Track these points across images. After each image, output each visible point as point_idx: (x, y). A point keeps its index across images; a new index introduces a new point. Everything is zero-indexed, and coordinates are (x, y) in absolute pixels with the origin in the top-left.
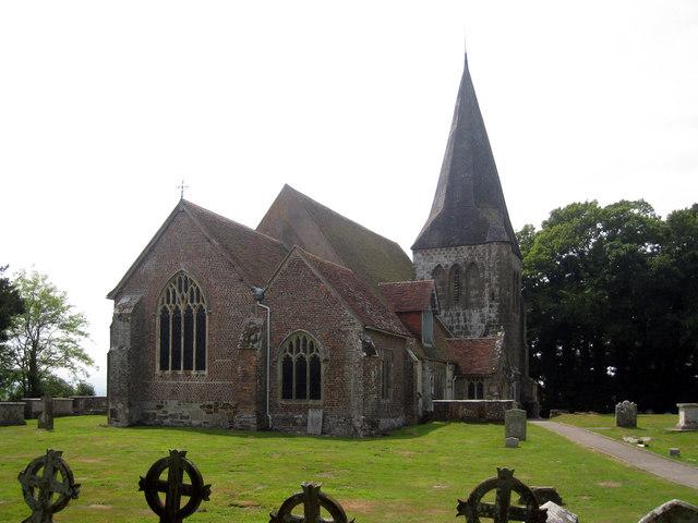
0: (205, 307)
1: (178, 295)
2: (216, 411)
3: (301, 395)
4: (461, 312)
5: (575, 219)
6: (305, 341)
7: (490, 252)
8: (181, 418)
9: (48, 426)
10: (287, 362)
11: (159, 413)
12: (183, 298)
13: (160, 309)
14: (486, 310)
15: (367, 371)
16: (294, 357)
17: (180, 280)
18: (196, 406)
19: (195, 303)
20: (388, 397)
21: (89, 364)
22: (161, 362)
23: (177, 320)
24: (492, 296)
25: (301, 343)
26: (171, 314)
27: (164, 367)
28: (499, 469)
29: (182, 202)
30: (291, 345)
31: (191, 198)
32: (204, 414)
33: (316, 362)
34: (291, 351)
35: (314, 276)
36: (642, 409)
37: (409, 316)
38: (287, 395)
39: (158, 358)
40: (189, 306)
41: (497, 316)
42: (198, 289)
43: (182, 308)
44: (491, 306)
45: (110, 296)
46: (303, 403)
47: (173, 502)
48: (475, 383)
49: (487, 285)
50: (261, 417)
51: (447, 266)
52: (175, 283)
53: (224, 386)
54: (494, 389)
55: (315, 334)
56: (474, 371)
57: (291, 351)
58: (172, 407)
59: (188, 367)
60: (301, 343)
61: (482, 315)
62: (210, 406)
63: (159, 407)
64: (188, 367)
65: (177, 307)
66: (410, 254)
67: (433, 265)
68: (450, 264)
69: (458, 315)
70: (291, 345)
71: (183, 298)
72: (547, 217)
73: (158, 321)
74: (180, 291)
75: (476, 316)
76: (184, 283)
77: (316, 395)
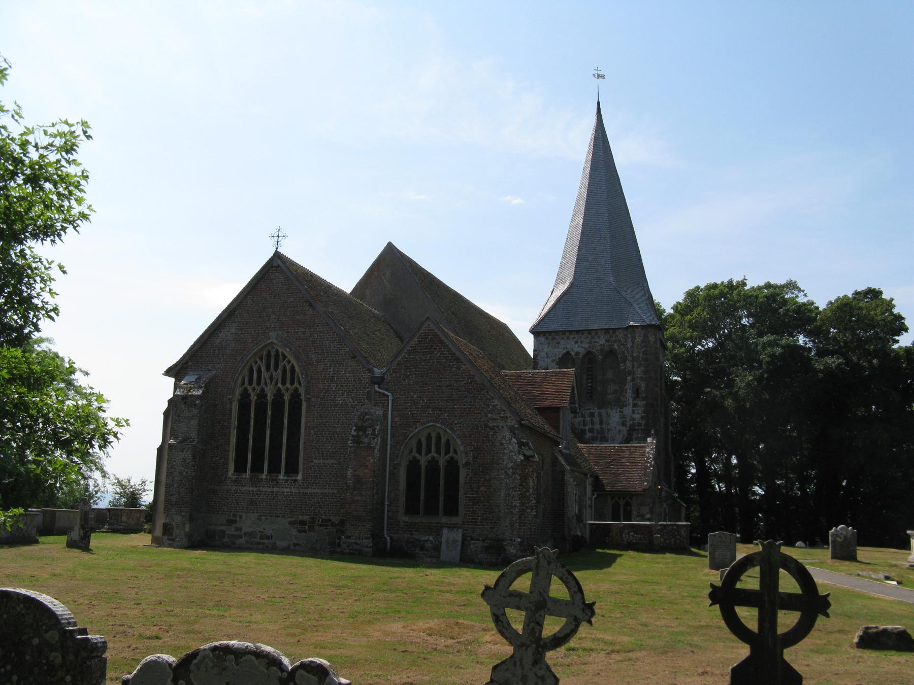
0: (302, 390)
2: (311, 528)
3: (431, 509)
4: (597, 411)
5: (716, 303)
6: (439, 438)
7: (634, 338)
8: (262, 537)
9: (82, 544)
10: (413, 466)
11: (231, 530)
12: (271, 378)
13: (238, 391)
14: (628, 410)
15: (524, 478)
16: (423, 460)
17: (269, 355)
19: (288, 385)
21: (130, 461)
22: (237, 461)
24: (637, 392)
25: (434, 440)
26: (253, 398)
27: (240, 467)
28: (711, 605)
29: (277, 256)
30: (419, 443)
31: (291, 252)
33: (453, 466)
34: (419, 451)
35: (453, 354)
37: (551, 413)
38: (412, 509)
39: (232, 455)
40: (279, 390)
42: (293, 369)
44: (635, 405)
45: (168, 373)
47: (570, 580)
48: (622, 502)
49: (629, 378)
50: (376, 536)
51: (577, 353)
52: (261, 358)
54: (645, 510)
55: (452, 429)
56: (619, 487)
57: (419, 451)
58: (248, 523)
59: (274, 469)
60: (434, 440)
62: (303, 523)
63: (231, 522)
64: (274, 469)
65: (263, 390)
66: (528, 343)
68: (582, 351)
69: (592, 415)
70: (419, 443)
71: (271, 378)
72: (680, 298)
73: (235, 407)
74: (268, 368)
75: (615, 417)
76: (272, 359)
77: (452, 509)
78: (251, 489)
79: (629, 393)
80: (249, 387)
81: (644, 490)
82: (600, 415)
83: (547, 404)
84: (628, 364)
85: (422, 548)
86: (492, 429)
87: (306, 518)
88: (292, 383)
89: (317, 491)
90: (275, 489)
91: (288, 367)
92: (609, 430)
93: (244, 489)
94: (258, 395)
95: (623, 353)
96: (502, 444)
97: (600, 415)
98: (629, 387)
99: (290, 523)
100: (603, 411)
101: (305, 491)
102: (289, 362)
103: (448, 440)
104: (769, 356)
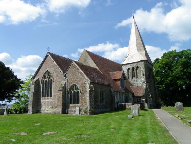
0: (52, 79)
1: (47, 77)
14: (142, 78)
18: (49, 107)
20: (103, 103)
22: (47, 95)
23: (46, 83)
24: (143, 74)
26: (45, 81)
32: (51, 109)
36: (185, 105)
43: (47, 80)
46: (75, 105)
49: (141, 72)
51: (131, 68)
53: (56, 101)
61: (141, 80)
62: (52, 107)
65: (46, 80)
67: (127, 68)
68: (132, 67)
69: (135, 80)
72: (162, 55)
74: (47, 76)
77: (78, 103)
79: (142, 75)
82: (136, 80)
84: (141, 69)
85: (73, 112)
86: (85, 84)
87: (53, 106)
94: (45, 81)
98: (142, 73)
99: (51, 107)
100: (137, 79)
104: (181, 65)
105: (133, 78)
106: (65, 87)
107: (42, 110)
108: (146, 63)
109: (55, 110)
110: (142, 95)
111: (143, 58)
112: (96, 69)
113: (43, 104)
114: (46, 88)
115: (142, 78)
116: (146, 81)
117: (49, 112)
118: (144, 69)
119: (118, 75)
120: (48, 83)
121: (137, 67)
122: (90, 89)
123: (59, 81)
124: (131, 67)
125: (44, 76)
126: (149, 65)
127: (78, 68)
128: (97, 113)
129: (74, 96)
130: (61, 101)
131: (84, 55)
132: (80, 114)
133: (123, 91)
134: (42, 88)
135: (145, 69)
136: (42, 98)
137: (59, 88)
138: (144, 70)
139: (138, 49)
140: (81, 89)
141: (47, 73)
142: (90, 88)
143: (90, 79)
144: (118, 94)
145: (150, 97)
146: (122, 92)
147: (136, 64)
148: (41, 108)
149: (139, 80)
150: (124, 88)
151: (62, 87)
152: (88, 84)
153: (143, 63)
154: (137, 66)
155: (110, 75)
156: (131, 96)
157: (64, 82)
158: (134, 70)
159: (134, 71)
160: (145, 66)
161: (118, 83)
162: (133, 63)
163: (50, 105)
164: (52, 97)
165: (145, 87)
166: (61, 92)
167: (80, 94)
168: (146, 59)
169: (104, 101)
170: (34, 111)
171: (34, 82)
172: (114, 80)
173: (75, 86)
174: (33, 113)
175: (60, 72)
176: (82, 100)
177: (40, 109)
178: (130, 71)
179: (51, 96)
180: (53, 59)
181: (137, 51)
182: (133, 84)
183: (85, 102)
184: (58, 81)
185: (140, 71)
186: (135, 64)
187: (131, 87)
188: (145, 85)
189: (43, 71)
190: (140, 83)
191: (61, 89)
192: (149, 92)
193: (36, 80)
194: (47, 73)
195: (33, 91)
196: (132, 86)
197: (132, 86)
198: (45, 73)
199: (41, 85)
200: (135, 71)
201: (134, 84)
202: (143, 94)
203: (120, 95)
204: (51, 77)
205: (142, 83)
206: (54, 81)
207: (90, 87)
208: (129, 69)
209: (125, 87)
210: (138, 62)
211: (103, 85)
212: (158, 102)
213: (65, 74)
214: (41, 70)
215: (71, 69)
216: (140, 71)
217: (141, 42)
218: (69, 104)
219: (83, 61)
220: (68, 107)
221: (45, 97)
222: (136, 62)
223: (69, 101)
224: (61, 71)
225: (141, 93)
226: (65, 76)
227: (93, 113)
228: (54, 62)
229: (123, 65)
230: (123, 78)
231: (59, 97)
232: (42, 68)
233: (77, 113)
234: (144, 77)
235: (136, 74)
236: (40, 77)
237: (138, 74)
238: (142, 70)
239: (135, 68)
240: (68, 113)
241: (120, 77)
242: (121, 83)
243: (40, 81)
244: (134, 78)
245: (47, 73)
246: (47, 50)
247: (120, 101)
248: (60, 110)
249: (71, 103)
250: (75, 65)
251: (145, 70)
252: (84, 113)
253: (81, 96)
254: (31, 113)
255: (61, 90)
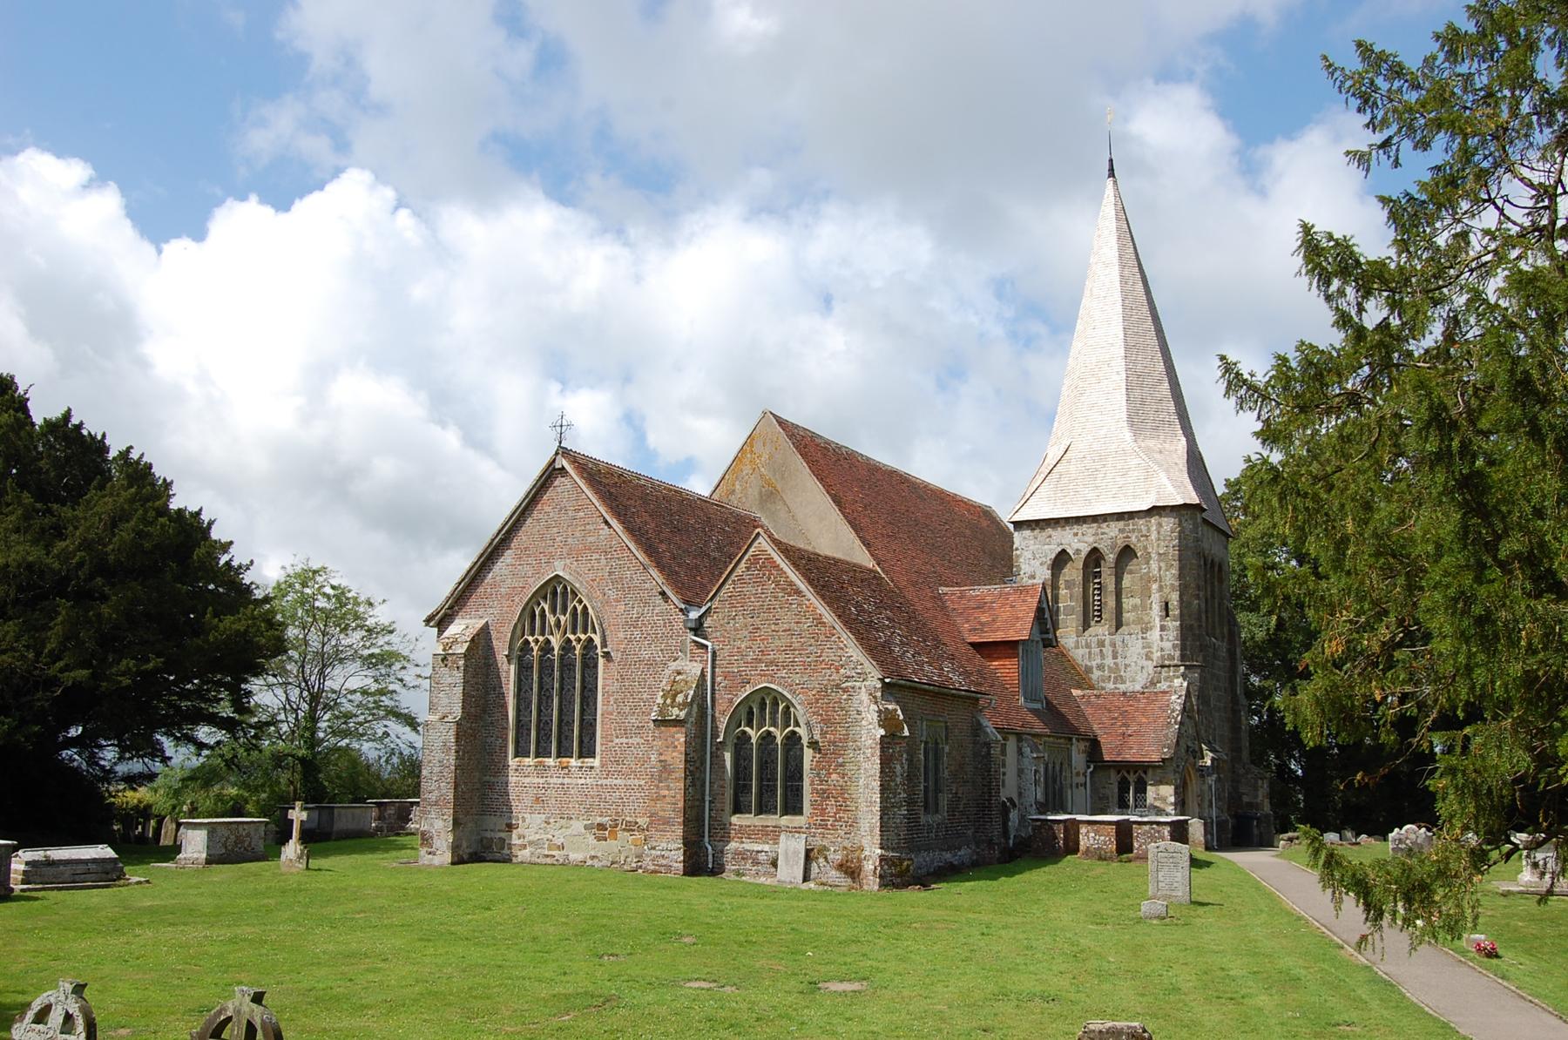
0: (597, 640)
1: (551, 619)
14: (1155, 634)
18: (578, 826)
22: (517, 743)
23: (545, 666)
32: (591, 839)
40: (569, 640)
41: (1174, 646)
43: (556, 642)
44: (1163, 628)
48: (1132, 778)
49: (1155, 586)
51: (1078, 551)
61: (1147, 646)
62: (601, 827)
67: (1052, 551)
68: (1085, 549)
69: (1101, 644)
74: (554, 611)
78: (536, 780)
80: (531, 639)
81: (1164, 760)
82: (1113, 645)
83: (998, 636)
84: (1154, 565)
85: (756, 863)
86: (845, 690)
87: (604, 820)
88: (585, 632)
89: (618, 782)
90: (566, 781)
91: (580, 608)
92: (1126, 666)
93: (527, 780)
94: (541, 649)
95: (1145, 548)
96: (859, 713)
97: (1113, 645)
99: (586, 827)
100: (1117, 638)
101: (604, 782)
102: (580, 601)
103: (787, 708)
105: (1086, 626)
106: (701, 706)
107: (515, 841)
108: (1189, 526)
109: (621, 846)
110: (1155, 757)
111: (1170, 488)
112: (877, 577)
113: (528, 801)
114: (550, 697)
115: (1155, 634)
116: (1183, 658)
117: (576, 856)
118: (1175, 571)
119: (1005, 614)
120: (567, 666)
121: (1127, 553)
122: (882, 732)
123: (648, 655)
124: (1076, 546)
125: (529, 615)
126: (1211, 544)
127: (791, 584)
128: (924, 879)
129: (766, 764)
130: (675, 790)
131: (758, 447)
132: (806, 878)
133: (1039, 727)
134: (531, 694)
135: (1181, 569)
136: (513, 762)
137: (663, 709)
138: (1171, 576)
139: (1137, 420)
140: (814, 720)
141: (555, 593)
142: (886, 719)
143: (882, 664)
144: (1012, 744)
145: (1203, 772)
146: (1034, 735)
147: (1121, 524)
148: (510, 827)
149: (1135, 648)
150: (1038, 706)
151: (680, 699)
152: (864, 697)
153: (1169, 524)
154: (1120, 544)
155: (944, 608)
156: (1078, 757)
157: (695, 669)
158: (1101, 569)
159: (1098, 575)
160: (1182, 548)
161: (1006, 669)
162: (1095, 519)
163: (582, 813)
164: (596, 762)
165: (1176, 701)
166: (681, 738)
167: (808, 754)
168: (1194, 498)
169: (944, 800)
170: (465, 845)
171: (461, 649)
172: (978, 647)
173: (775, 704)
174: (461, 858)
175: (659, 600)
176: (824, 795)
177: (503, 835)
178: (1073, 572)
179: (587, 751)
180: (597, 492)
181: (1128, 435)
182: (1089, 670)
183: (840, 808)
184: (645, 654)
185: (1148, 580)
186: (1112, 530)
187: (1075, 692)
188: (1180, 684)
189: (515, 578)
190: (1137, 665)
191: (675, 711)
192: (1199, 738)
193: (473, 640)
194: (556, 591)
195: (457, 712)
196: (1083, 681)
197: (1079, 687)
198: (540, 594)
199: (509, 674)
200: (1108, 580)
201: (1096, 674)
202: (1167, 753)
203: (1020, 752)
204: (581, 620)
205: (1150, 665)
206: (607, 655)
207: (880, 711)
208: (1061, 559)
209: (1049, 703)
210: (1131, 515)
211: (936, 694)
212: (1246, 799)
213: (694, 615)
214: (501, 567)
215: (739, 581)
216: (1148, 580)
217: (1161, 367)
218: (728, 807)
219: (754, 492)
220: (722, 833)
221: (542, 752)
222: (1120, 516)
223: (729, 793)
224: (663, 594)
225: (1151, 740)
226: (698, 628)
227: (897, 876)
228: (614, 522)
229: (1019, 525)
230: (1037, 637)
231: (665, 767)
232: (508, 557)
233: (790, 871)
234: (1173, 625)
235: (1111, 602)
236: (495, 612)
237: (1128, 603)
238: (1158, 578)
239: (1111, 557)
240: (717, 870)
241: (1021, 630)
242: (1025, 674)
243: (501, 649)
244: (1100, 630)
245: (556, 591)
246: (554, 434)
247: (1020, 794)
248: (671, 847)
249: (738, 809)
250: (770, 559)
251: (1181, 576)
252: (834, 875)
253: (817, 769)
254: (448, 857)
255: (677, 723)
